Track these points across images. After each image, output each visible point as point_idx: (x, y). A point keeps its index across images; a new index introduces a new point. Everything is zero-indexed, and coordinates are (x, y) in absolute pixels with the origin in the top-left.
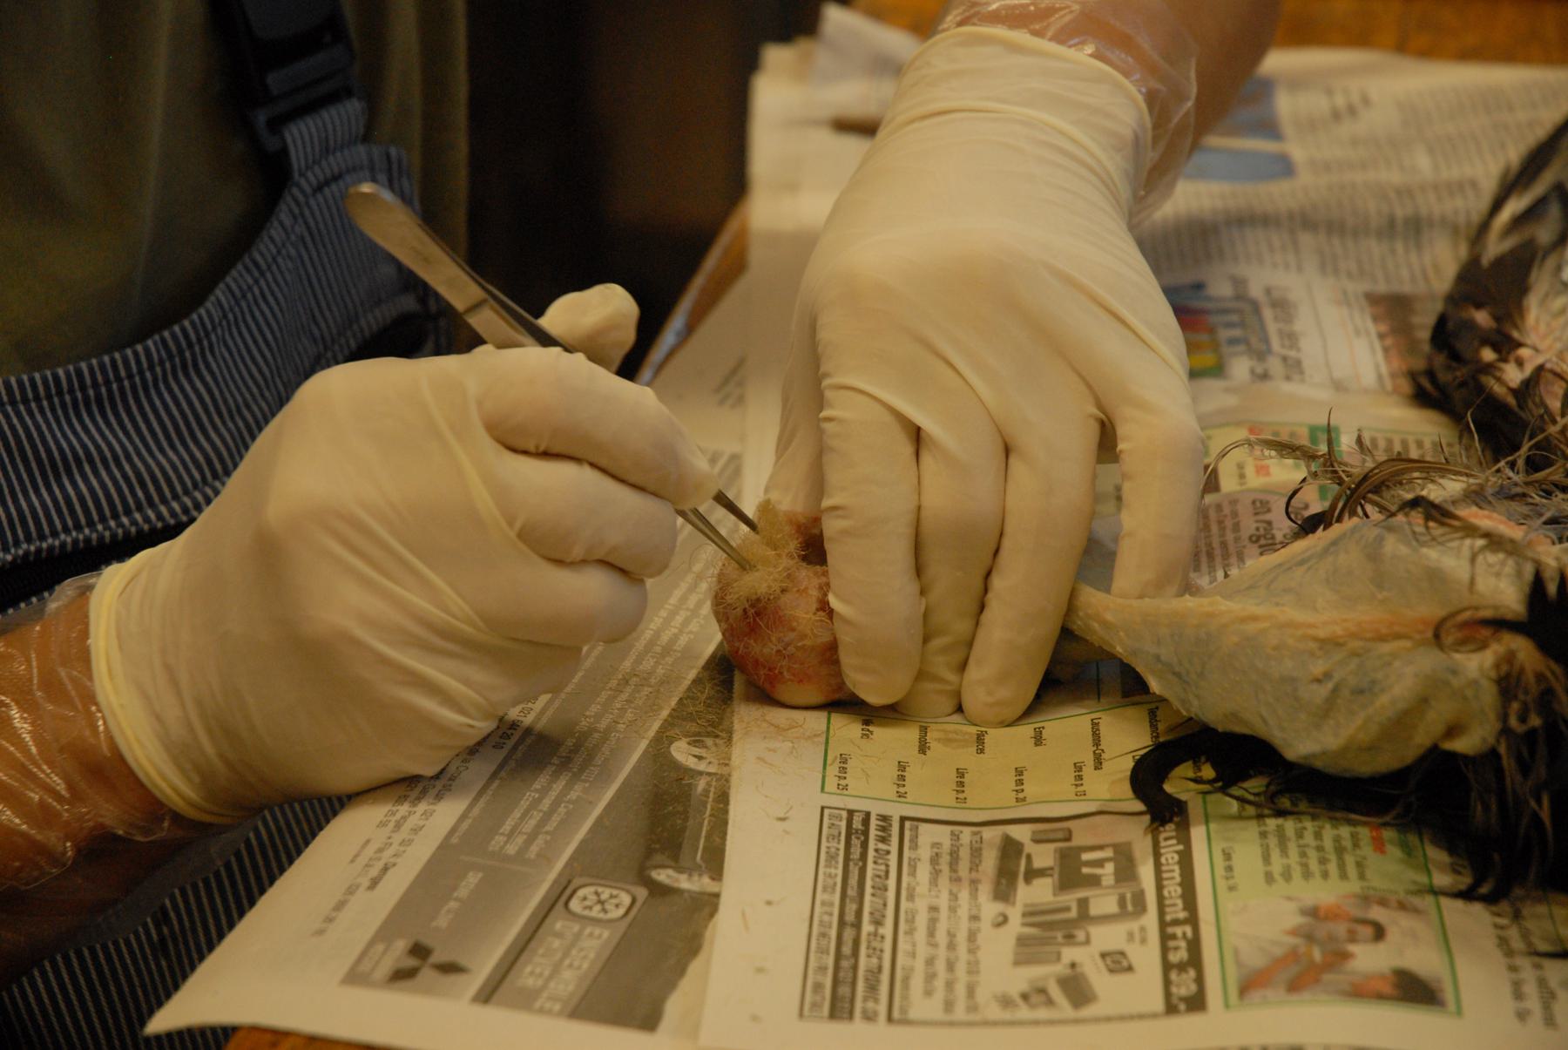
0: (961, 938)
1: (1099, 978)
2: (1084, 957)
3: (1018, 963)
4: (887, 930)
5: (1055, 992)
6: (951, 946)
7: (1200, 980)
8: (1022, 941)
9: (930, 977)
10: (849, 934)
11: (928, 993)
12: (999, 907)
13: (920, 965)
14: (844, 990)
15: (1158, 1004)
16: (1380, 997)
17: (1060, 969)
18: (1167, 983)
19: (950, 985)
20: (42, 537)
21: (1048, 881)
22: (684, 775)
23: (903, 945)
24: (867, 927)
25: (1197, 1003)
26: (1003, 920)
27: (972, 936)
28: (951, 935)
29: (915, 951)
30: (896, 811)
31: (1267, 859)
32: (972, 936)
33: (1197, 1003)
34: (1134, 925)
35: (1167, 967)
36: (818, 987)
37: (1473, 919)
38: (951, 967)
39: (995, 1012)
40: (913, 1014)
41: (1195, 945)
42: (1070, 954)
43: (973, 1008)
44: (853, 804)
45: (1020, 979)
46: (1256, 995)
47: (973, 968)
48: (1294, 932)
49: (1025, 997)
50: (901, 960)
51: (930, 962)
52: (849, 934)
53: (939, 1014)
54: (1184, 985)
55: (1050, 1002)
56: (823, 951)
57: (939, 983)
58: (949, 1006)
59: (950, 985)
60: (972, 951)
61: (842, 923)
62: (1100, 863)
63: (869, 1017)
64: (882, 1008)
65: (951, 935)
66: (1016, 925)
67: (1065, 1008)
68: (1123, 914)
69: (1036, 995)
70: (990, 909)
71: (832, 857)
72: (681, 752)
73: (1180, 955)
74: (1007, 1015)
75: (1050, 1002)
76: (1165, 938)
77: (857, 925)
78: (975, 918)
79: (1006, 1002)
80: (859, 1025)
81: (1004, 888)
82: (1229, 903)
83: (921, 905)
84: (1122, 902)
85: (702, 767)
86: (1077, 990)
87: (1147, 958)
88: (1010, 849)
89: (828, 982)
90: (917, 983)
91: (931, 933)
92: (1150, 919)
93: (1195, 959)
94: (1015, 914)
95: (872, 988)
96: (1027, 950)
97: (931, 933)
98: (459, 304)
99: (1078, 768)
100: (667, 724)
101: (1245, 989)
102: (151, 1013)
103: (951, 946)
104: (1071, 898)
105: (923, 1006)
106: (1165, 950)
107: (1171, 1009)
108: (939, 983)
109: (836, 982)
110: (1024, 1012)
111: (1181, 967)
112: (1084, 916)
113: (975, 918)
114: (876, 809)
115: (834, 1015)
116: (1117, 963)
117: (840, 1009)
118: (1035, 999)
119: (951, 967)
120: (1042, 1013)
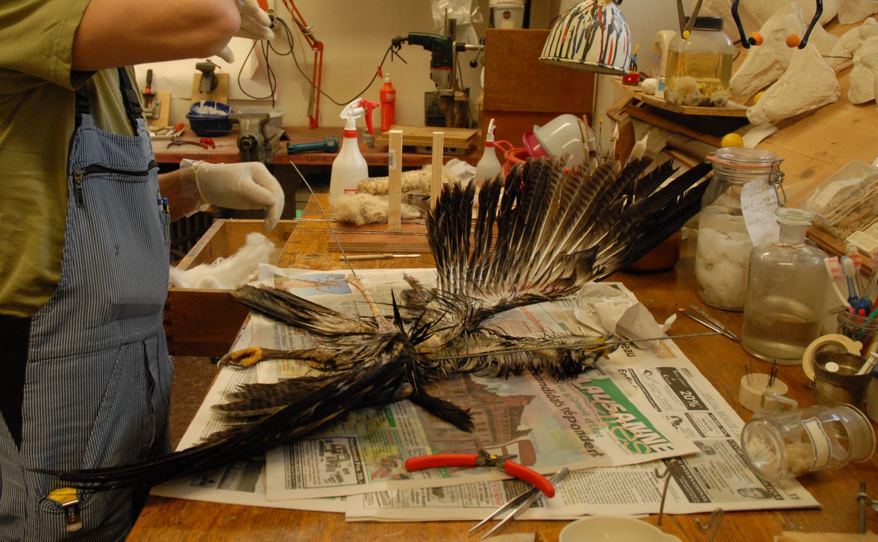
5: (335, 479)
20: (573, 193)
21: (507, 447)
25: (363, 481)
26: (322, 460)
33: (363, 481)
35: (357, 472)
37: (806, 466)
39: (323, 484)
40: (308, 486)
41: (361, 467)
42: (337, 469)
45: (328, 475)
46: (375, 479)
53: (313, 485)
54: (361, 478)
58: (315, 483)
66: (325, 462)
67: (338, 483)
68: (346, 459)
69: (331, 479)
73: (359, 469)
76: (355, 465)
80: (298, 489)
87: (352, 470)
90: (308, 478)
93: (362, 471)
94: (324, 458)
96: (330, 468)
98: (474, 205)
101: (373, 478)
104: (335, 455)
105: (310, 484)
107: (359, 483)
110: (330, 484)
111: (359, 472)
116: (346, 471)
117: (294, 486)
120: (333, 484)
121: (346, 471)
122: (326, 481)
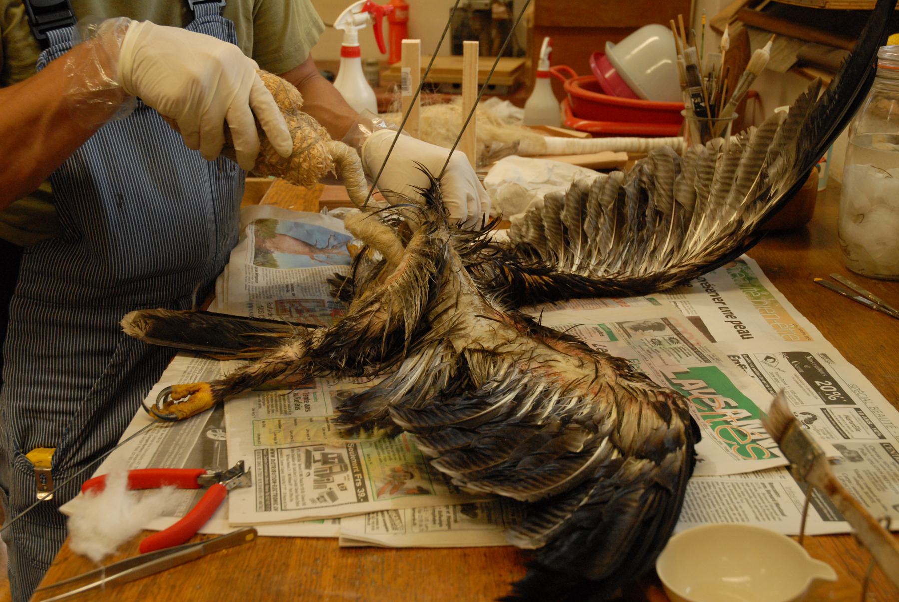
0: (298, 481)
1: (338, 492)
2: (333, 486)
3: (316, 487)
4: (277, 483)
5: (326, 497)
6: (296, 484)
7: (365, 492)
8: (315, 481)
9: (291, 495)
10: (267, 487)
11: (291, 500)
12: (308, 470)
13: (288, 491)
14: (268, 502)
15: (355, 499)
16: (414, 494)
17: (326, 490)
18: (357, 493)
19: (297, 497)
22: (212, 442)
23: (282, 486)
24: (272, 484)
25: (366, 499)
27: (301, 481)
28: (295, 481)
29: (286, 489)
30: (274, 447)
31: (379, 455)
32: (301, 481)
33: (366, 499)
34: (345, 474)
35: (356, 488)
36: (260, 502)
38: (296, 490)
39: (309, 504)
40: (288, 507)
42: (329, 485)
43: (304, 504)
44: (262, 447)
45: (316, 493)
46: (382, 496)
47: (303, 491)
48: (389, 476)
49: (318, 499)
50: (283, 491)
51: (290, 490)
52: (267, 487)
55: (325, 500)
56: (260, 492)
57: (294, 496)
58: (297, 504)
59: (297, 497)
60: (303, 492)
61: (265, 485)
62: (333, 458)
63: (276, 509)
64: (279, 506)
65: (295, 481)
66: (313, 477)
69: (321, 498)
70: (305, 471)
71: (259, 463)
72: (210, 434)
74: (313, 505)
75: (325, 500)
76: (355, 478)
77: (269, 484)
78: (301, 475)
79: (313, 501)
81: (308, 466)
82: (370, 466)
83: (286, 472)
84: (341, 467)
85: (216, 438)
86: (332, 496)
87: (350, 484)
88: (308, 453)
89: (263, 500)
90: (288, 497)
91: (290, 481)
92: (349, 472)
94: (312, 471)
95: (276, 501)
96: (318, 484)
97: (290, 481)
99: (324, 430)
100: (206, 426)
101: (378, 495)
102: (62, 504)
103: (296, 484)
105: (290, 505)
106: (355, 482)
107: (359, 501)
108: (294, 496)
109: (265, 501)
110: (318, 504)
111: (360, 488)
112: (331, 472)
113: (301, 475)
114: (269, 448)
115: (265, 510)
116: (342, 487)
118: (321, 499)
119: (296, 490)
120: (324, 504)
121: (342, 487)
122: (313, 501)
